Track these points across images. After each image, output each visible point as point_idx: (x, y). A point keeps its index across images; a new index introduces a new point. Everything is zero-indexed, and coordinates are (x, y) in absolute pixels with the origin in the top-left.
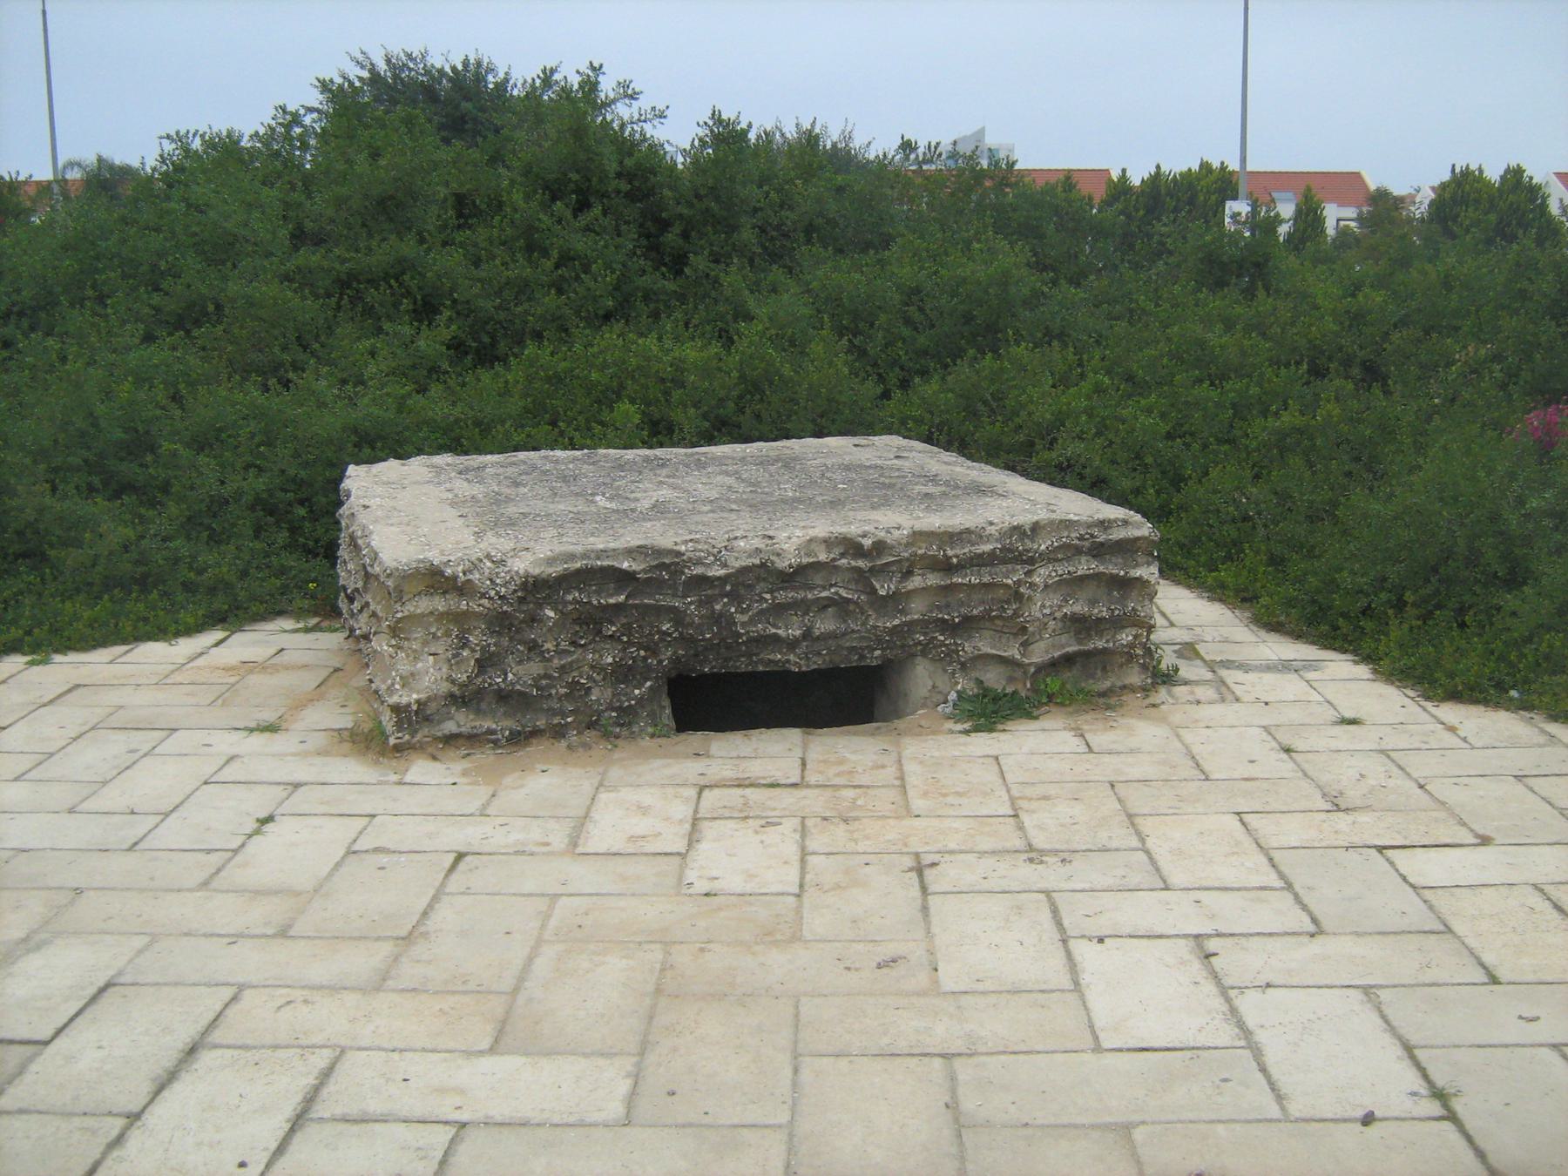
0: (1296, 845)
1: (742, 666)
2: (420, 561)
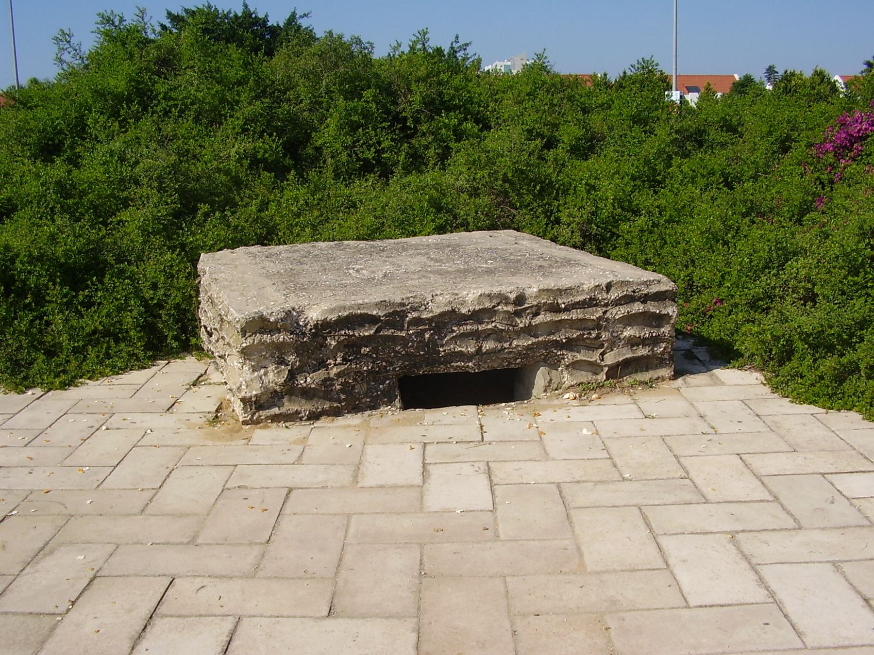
0: (776, 473)
1: (441, 369)
2: (256, 313)
